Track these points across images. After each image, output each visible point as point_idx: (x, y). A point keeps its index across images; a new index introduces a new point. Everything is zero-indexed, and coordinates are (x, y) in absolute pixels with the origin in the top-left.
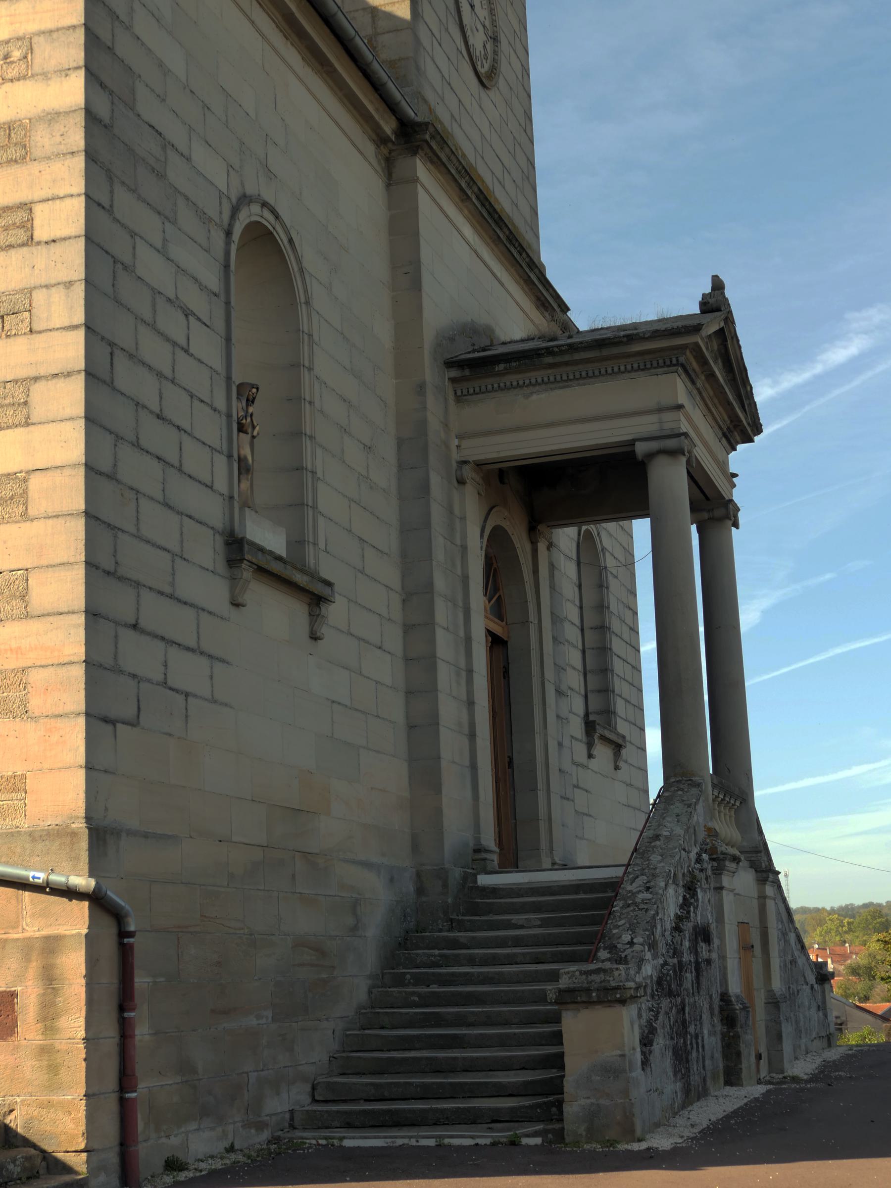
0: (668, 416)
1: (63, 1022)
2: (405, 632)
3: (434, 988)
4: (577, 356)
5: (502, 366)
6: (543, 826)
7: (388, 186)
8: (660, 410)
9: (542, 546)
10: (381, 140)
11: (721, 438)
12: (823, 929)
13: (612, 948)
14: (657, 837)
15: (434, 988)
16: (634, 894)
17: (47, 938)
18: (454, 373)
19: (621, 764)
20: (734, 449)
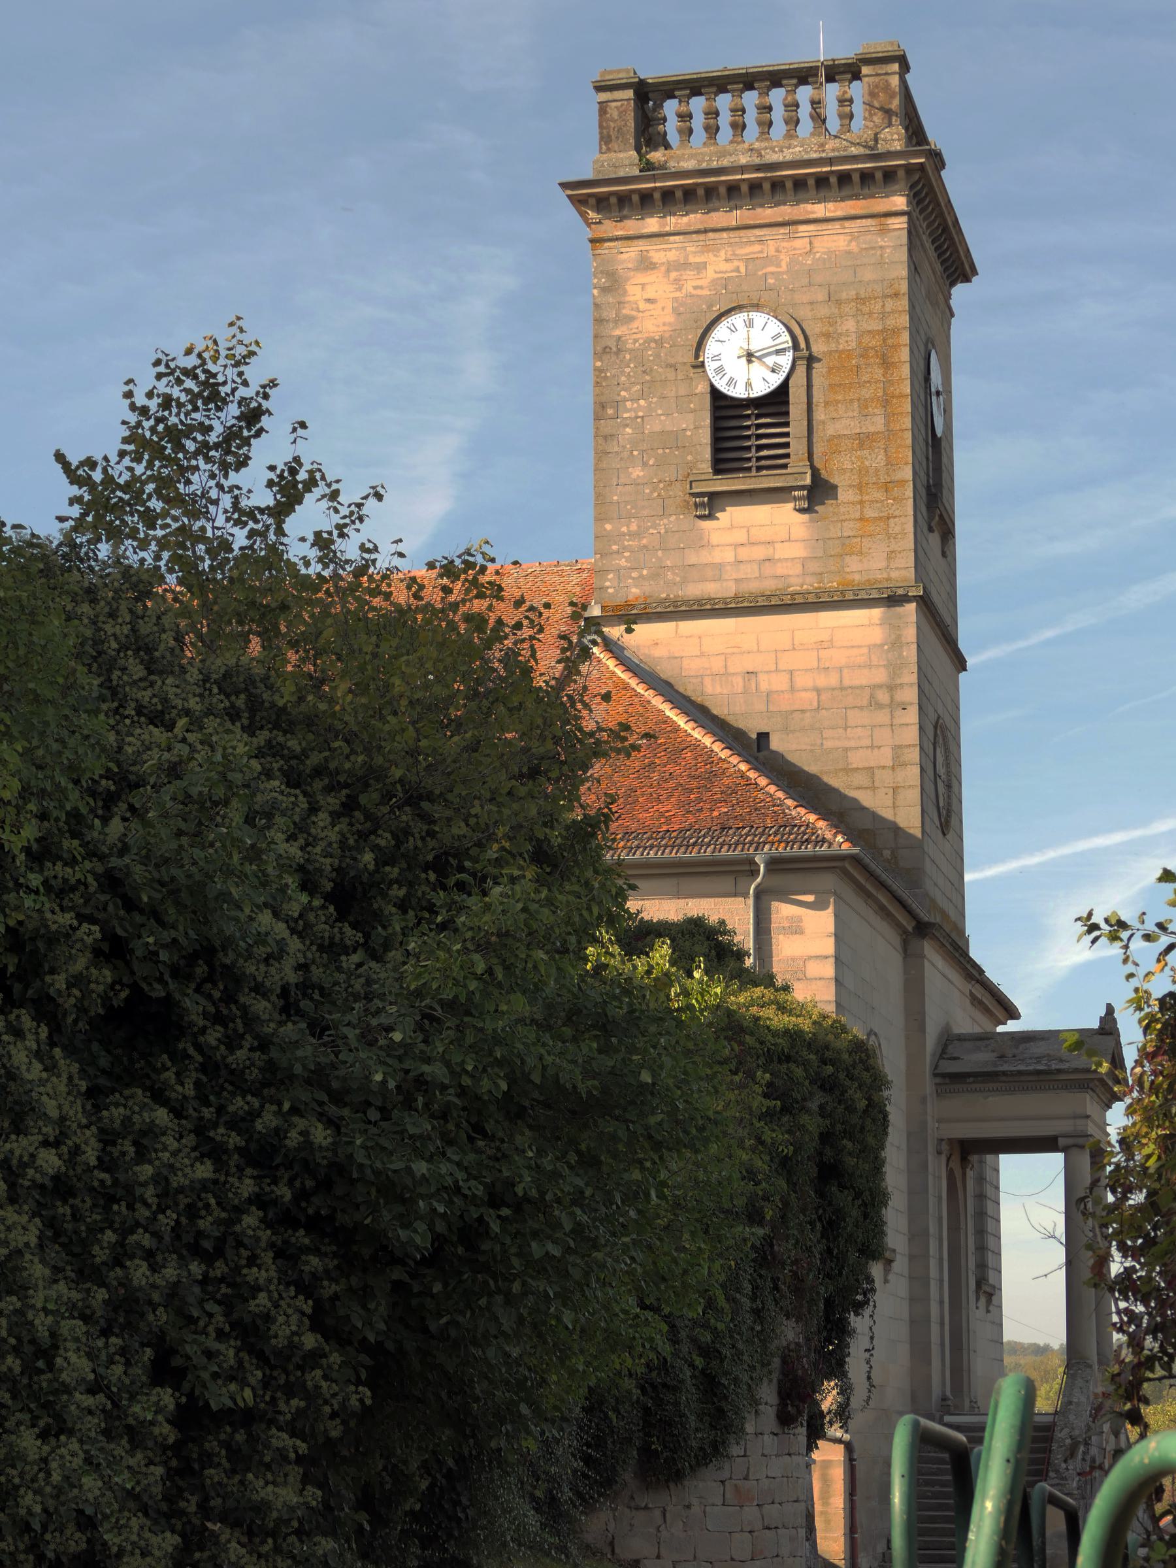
0: (1079, 1122)
1: (832, 1500)
2: (910, 1260)
3: (937, 1488)
4: (1022, 1078)
5: (972, 1079)
6: (965, 1374)
7: (904, 958)
8: (1075, 1117)
9: (970, 1174)
10: (905, 932)
11: (760, 155)
12: (1051, 1388)
13: (1057, 1471)
14: (1070, 1403)
15: (937, 1488)
16: (1063, 1440)
17: (824, 1461)
18: (938, 1080)
19: (991, 1308)
20: (1110, 1107)
